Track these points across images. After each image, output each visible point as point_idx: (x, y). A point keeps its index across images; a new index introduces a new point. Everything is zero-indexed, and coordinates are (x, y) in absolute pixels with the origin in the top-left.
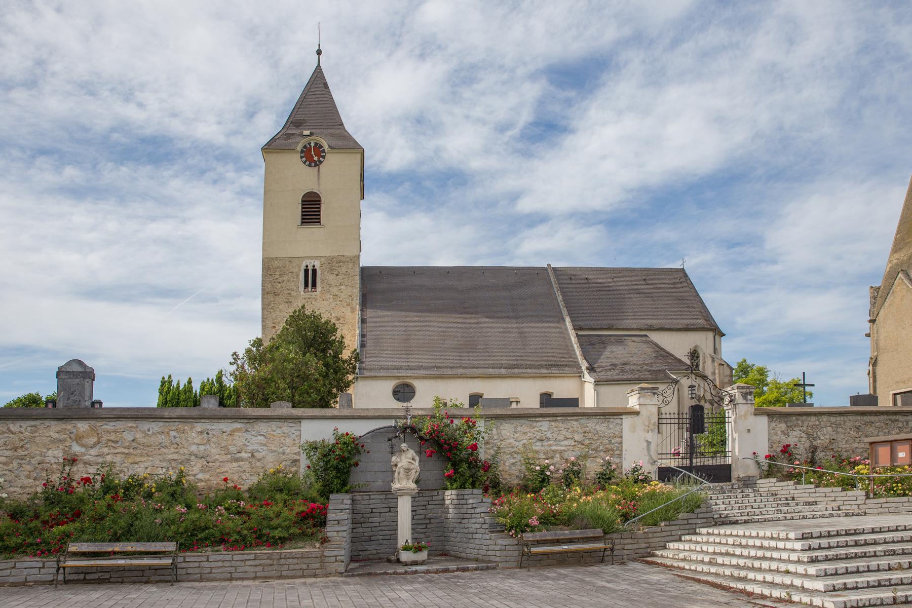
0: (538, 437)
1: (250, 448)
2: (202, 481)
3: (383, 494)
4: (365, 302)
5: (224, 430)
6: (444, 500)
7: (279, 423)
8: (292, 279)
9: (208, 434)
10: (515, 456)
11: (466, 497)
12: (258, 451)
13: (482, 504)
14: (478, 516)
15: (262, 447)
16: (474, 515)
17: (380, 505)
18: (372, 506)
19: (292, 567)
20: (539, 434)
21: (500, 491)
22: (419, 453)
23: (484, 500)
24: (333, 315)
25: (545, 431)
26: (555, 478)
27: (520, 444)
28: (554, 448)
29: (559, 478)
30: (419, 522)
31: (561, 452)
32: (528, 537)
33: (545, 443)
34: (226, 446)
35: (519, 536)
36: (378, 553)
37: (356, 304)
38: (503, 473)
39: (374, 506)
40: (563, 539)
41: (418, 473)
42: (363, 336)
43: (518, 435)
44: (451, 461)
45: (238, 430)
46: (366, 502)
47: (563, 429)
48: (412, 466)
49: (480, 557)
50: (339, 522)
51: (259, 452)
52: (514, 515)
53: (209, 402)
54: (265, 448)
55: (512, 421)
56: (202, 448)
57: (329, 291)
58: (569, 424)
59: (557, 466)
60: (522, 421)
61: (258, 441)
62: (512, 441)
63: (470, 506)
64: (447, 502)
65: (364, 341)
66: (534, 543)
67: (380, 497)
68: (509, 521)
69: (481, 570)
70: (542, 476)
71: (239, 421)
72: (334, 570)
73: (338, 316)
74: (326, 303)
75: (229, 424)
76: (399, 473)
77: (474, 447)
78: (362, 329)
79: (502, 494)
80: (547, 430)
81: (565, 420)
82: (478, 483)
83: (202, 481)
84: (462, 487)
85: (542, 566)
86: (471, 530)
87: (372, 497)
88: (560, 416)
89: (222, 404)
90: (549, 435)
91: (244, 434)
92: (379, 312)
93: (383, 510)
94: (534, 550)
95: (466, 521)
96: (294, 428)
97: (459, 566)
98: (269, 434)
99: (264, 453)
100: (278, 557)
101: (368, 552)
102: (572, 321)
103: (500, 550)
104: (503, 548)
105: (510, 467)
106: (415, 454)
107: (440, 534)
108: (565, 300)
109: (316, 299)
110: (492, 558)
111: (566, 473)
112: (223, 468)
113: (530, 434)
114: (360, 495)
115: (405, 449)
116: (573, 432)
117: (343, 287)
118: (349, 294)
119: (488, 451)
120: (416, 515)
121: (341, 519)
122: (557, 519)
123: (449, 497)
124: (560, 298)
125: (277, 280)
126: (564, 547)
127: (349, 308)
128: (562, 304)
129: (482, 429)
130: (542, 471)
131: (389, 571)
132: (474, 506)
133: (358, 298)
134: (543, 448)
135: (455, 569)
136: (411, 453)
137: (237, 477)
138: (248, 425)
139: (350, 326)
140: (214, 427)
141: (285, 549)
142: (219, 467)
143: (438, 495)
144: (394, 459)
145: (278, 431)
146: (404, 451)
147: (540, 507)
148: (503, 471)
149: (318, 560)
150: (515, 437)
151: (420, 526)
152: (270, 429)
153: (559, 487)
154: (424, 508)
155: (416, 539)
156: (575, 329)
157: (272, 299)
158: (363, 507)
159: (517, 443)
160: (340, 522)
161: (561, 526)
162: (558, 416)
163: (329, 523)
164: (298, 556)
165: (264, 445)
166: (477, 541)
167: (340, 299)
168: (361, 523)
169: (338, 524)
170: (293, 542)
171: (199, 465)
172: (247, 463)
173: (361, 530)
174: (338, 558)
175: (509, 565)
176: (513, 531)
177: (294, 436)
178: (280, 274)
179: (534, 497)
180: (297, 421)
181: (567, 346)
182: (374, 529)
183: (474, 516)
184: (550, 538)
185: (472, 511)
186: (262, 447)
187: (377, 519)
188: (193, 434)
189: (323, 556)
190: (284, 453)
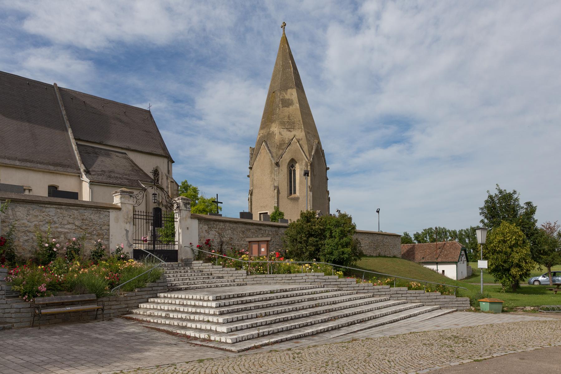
10: (28, 234)
20: (48, 218)
21: (15, 263)
25: (52, 216)
28: (59, 230)
31: (65, 233)
32: (39, 301)
40: (66, 302)
47: (66, 215)
52: (27, 283)
55: (25, 205)
59: (62, 244)
60: (34, 206)
68: (22, 288)
79: (17, 265)
80: (54, 215)
88: (64, 205)
94: (43, 311)
102: (74, 132)
103: (16, 312)
104: (18, 310)
108: (67, 115)
116: (74, 218)
119: (5, 229)
124: (64, 113)
126: (67, 308)
128: (65, 117)
130: (50, 248)
150: (28, 218)
156: (75, 139)
159: (30, 224)
161: (65, 292)
176: (26, 296)
184: (57, 301)
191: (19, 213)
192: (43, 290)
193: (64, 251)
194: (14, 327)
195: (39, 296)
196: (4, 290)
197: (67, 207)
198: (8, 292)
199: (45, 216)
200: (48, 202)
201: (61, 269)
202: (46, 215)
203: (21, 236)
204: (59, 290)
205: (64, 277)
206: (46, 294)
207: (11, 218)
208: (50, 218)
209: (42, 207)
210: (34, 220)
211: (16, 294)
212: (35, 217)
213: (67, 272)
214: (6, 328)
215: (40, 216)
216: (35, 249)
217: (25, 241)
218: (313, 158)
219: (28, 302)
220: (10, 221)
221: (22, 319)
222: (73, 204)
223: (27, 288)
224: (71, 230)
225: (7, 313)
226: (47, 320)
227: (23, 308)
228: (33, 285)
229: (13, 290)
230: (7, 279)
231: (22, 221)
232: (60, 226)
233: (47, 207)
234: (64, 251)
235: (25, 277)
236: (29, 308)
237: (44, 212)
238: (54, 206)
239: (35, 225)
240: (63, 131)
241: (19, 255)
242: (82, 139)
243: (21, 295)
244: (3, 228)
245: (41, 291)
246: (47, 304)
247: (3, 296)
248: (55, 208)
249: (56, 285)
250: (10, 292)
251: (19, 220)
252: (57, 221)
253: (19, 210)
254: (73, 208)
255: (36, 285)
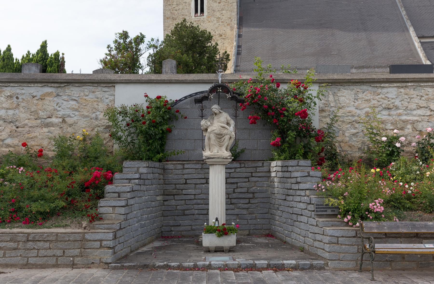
0: (383, 105)
1: (61, 113)
2: (11, 146)
3: (198, 163)
4: (241, 22)
5: (34, 94)
6: (269, 172)
7: (92, 87)
8: (185, 7)
9: (17, 98)
10: (357, 125)
11: (290, 169)
12: (69, 116)
13: (309, 178)
14: (303, 193)
15: (74, 113)
16: (299, 191)
17: (195, 176)
18: (186, 176)
19: (42, 252)
20: (386, 101)
21: (336, 164)
22: (235, 117)
23: (312, 173)
24: (217, 33)
25: (392, 99)
26: (407, 152)
27: (362, 113)
28: (404, 118)
29: (411, 153)
30: (241, 196)
31: (413, 123)
32: (371, 228)
33: (393, 112)
34: (36, 111)
35: (358, 224)
36: (192, 230)
37: (235, 24)
38: (342, 144)
39: (189, 176)
40: (424, 233)
41: (232, 140)
42: (239, 47)
43: (360, 102)
44: (277, 129)
45: (49, 94)
46: (179, 172)
47: (415, 96)
48: (225, 131)
49: (306, 247)
50: (119, 194)
51: (71, 117)
52: (351, 195)
53: (30, 70)
54: (77, 113)
55: (352, 87)
56: (11, 112)
57: (213, 15)
58: (423, 91)
59: (409, 138)
60: (364, 87)
61: (69, 106)
62: (352, 109)
63: (293, 180)
64: (273, 174)
65: (240, 51)
66: (379, 236)
67: (195, 167)
68: (343, 203)
69: (303, 269)
70: (390, 149)
71: (49, 85)
72: (98, 258)
73: (221, 33)
74: (211, 24)
75: (40, 88)
76: (209, 139)
77: (304, 114)
78: (238, 42)
79: (340, 167)
80: (394, 97)
81: (417, 86)
82: (310, 154)
83: (11, 146)
84: (292, 157)
85: (392, 270)
86: (296, 210)
87: (186, 166)
88: (411, 82)
89: (44, 71)
90: (397, 103)
91: (55, 99)
92: (253, 29)
93: (198, 181)
94: (380, 247)
95: (291, 198)
96: (108, 93)
97: (271, 262)
98: (81, 99)
99: (75, 118)
100: (24, 239)
101: (181, 228)
102: (416, 30)
103: (330, 243)
104: (334, 240)
105: (351, 138)
106: (229, 118)
107: (265, 210)
108: (408, 14)
109: (204, 21)
110: (320, 252)
111: (421, 146)
112: (33, 134)
113: (373, 102)
114: (172, 164)
115: (217, 111)
116: (428, 100)
117: (224, 12)
118: (229, 16)
119: (324, 120)
120: (237, 187)
121: (122, 191)
122: (412, 203)
123: (274, 169)
124: (404, 13)
125: (175, 9)
126: (427, 246)
127: (229, 27)
128: (405, 18)
129: (315, 94)
130: (391, 142)
131: (173, 264)
132: (299, 180)
133: (236, 19)
134: (391, 118)
135: (265, 266)
136: (225, 116)
137: (47, 143)
138: (60, 89)
139: (230, 41)
140: (23, 91)
141: (44, 228)
142: (29, 132)
143: (263, 166)
144: (203, 122)
145: (91, 96)
146: (216, 114)
147: (387, 186)
148: (342, 142)
149: (77, 244)
150: (356, 104)
151: (242, 201)
152: (82, 94)
153: (413, 162)
154: (247, 180)
155: (238, 215)
156: (419, 38)
157: (171, 23)
158: (176, 177)
159: (358, 112)
160: (122, 195)
161: (420, 213)
162: (408, 82)
163: (107, 195)
164: (51, 238)
165: (76, 110)
166: (302, 226)
167: (222, 21)
168: (174, 195)
169: (119, 197)
170: (61, 217)
171: (8, 130)
172: (58, 128)
173: (173, 202)
174: (104, 243)
175: (343, 265)
176: (349, 217)
177: (107, 101)
178: (177, 4)
179: (380, 172)
180: (111, 85)
181: (411, 50)
182: (188, 202)
183: (298, 193)
184: (405, 231)
185: (296, 187)
186: (74, 113)
187: (192, 191)
188: (2, 98)
189: (84, 240)
190: (97, 119)
191: (344, 98)
192: (378, 210)
193: (413, 148)
194: (328, 266)
195: (371, 217)
196: (313, 204)
197: (417, 84)
198: (319, 208)
199: (382, 100)
200: (385, 80)
201: (410, 175)
202: (383, 99)
203: (347, 128)
204: (409, 208)
205: (416, 188)
206: (383, 216)
207: (332, 105)
208: (389, 102)
209: (376, 87)
210: (364, 106)
211: (332, 211)
212: (366, 102)
213: (421, 180)
214: (315, 267)
215: (374, 99)
216: (367, 145)
217: (353, 134)
218: (167, 245)
219: (352, 226)
220: (331, 109)
221: (342, 255)
222: (426, 78)
223: (350, 203)
224: (423, 117)
225: (318, 241)
226: (387, 261)
227: (342, 237)
228: (361, 199)
229: (326, 205)
230: (318, 187)
231: (347, 109)
232: (405, 112)
233: (383, 87)
234: (413, 148)
235: (348, 184)
236: (354, 237)
237: (379, 95)
238: (395, 85)
239: (366, 113)
240: (404, 31)
241: (343, 154)
242: (426, 35)
243: (340, 214)
244: (322, 120)
245: (375, 211)
246: (386, 234)
247: (313, 213)
248: (396, 87)
249: (402, 199)
250: (323, 208)
251: (343, 107)
252: (401, 106)
253: (343, 95)
254: (426, 84)
255: (366, 199)
